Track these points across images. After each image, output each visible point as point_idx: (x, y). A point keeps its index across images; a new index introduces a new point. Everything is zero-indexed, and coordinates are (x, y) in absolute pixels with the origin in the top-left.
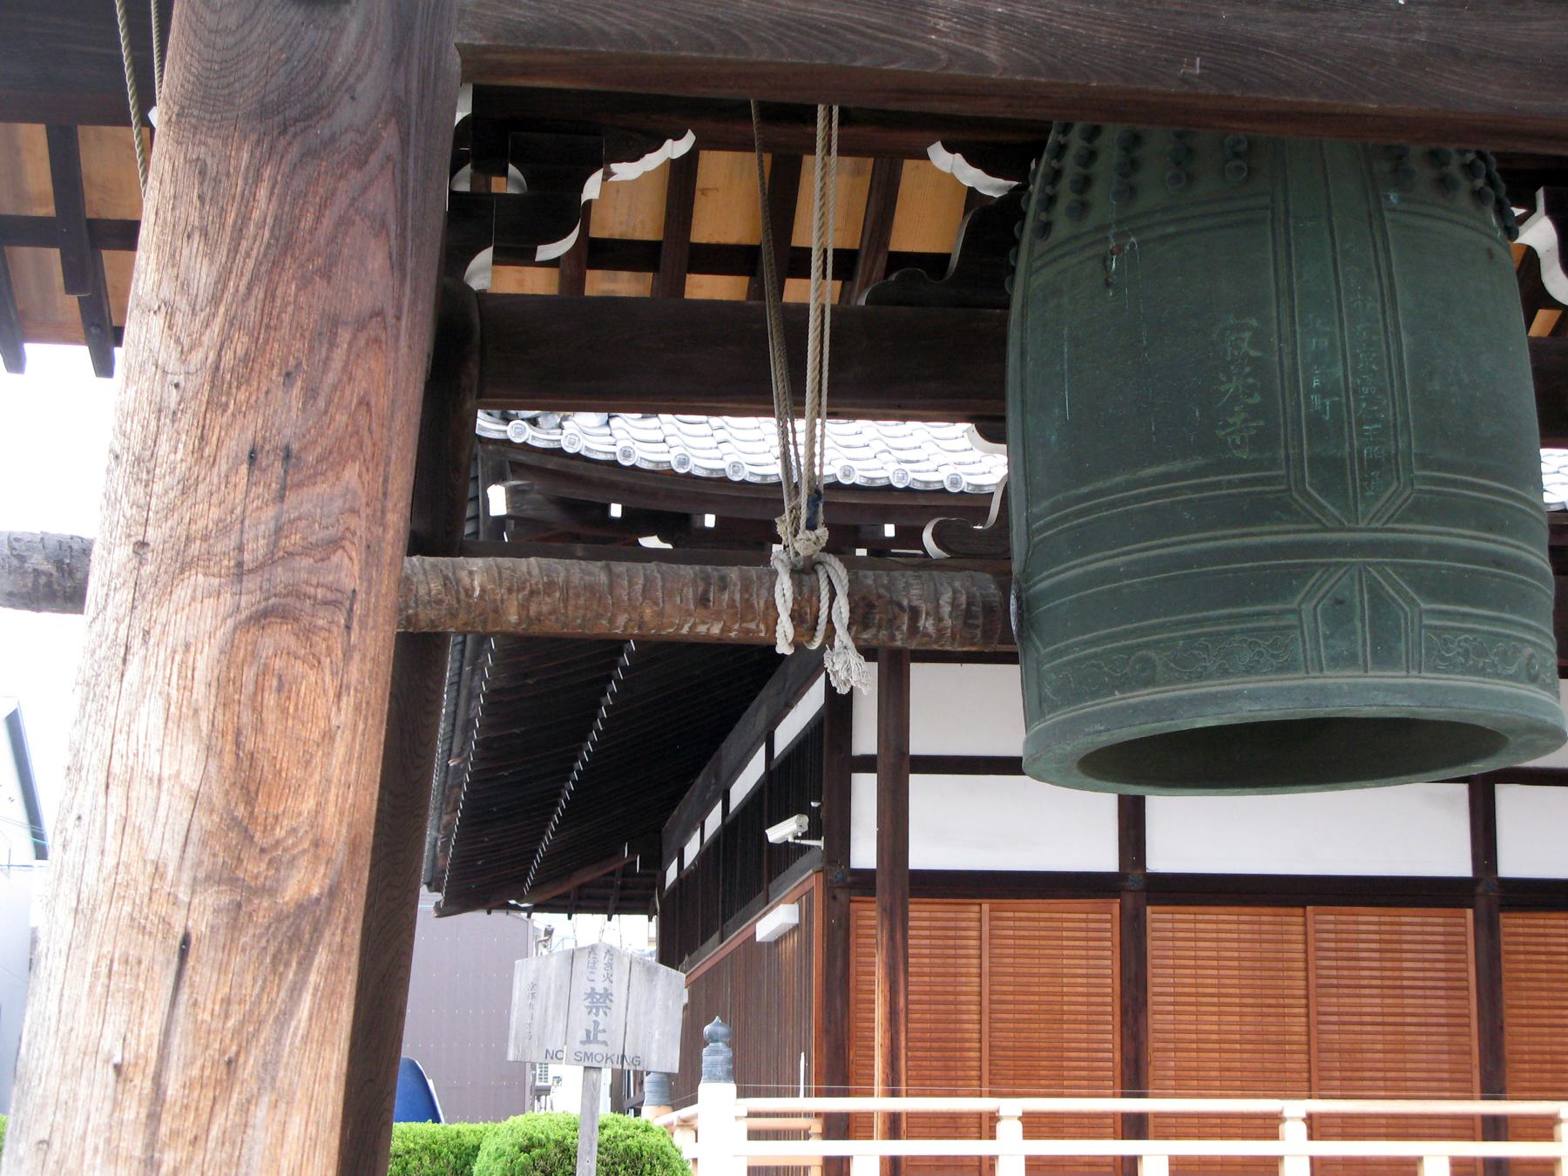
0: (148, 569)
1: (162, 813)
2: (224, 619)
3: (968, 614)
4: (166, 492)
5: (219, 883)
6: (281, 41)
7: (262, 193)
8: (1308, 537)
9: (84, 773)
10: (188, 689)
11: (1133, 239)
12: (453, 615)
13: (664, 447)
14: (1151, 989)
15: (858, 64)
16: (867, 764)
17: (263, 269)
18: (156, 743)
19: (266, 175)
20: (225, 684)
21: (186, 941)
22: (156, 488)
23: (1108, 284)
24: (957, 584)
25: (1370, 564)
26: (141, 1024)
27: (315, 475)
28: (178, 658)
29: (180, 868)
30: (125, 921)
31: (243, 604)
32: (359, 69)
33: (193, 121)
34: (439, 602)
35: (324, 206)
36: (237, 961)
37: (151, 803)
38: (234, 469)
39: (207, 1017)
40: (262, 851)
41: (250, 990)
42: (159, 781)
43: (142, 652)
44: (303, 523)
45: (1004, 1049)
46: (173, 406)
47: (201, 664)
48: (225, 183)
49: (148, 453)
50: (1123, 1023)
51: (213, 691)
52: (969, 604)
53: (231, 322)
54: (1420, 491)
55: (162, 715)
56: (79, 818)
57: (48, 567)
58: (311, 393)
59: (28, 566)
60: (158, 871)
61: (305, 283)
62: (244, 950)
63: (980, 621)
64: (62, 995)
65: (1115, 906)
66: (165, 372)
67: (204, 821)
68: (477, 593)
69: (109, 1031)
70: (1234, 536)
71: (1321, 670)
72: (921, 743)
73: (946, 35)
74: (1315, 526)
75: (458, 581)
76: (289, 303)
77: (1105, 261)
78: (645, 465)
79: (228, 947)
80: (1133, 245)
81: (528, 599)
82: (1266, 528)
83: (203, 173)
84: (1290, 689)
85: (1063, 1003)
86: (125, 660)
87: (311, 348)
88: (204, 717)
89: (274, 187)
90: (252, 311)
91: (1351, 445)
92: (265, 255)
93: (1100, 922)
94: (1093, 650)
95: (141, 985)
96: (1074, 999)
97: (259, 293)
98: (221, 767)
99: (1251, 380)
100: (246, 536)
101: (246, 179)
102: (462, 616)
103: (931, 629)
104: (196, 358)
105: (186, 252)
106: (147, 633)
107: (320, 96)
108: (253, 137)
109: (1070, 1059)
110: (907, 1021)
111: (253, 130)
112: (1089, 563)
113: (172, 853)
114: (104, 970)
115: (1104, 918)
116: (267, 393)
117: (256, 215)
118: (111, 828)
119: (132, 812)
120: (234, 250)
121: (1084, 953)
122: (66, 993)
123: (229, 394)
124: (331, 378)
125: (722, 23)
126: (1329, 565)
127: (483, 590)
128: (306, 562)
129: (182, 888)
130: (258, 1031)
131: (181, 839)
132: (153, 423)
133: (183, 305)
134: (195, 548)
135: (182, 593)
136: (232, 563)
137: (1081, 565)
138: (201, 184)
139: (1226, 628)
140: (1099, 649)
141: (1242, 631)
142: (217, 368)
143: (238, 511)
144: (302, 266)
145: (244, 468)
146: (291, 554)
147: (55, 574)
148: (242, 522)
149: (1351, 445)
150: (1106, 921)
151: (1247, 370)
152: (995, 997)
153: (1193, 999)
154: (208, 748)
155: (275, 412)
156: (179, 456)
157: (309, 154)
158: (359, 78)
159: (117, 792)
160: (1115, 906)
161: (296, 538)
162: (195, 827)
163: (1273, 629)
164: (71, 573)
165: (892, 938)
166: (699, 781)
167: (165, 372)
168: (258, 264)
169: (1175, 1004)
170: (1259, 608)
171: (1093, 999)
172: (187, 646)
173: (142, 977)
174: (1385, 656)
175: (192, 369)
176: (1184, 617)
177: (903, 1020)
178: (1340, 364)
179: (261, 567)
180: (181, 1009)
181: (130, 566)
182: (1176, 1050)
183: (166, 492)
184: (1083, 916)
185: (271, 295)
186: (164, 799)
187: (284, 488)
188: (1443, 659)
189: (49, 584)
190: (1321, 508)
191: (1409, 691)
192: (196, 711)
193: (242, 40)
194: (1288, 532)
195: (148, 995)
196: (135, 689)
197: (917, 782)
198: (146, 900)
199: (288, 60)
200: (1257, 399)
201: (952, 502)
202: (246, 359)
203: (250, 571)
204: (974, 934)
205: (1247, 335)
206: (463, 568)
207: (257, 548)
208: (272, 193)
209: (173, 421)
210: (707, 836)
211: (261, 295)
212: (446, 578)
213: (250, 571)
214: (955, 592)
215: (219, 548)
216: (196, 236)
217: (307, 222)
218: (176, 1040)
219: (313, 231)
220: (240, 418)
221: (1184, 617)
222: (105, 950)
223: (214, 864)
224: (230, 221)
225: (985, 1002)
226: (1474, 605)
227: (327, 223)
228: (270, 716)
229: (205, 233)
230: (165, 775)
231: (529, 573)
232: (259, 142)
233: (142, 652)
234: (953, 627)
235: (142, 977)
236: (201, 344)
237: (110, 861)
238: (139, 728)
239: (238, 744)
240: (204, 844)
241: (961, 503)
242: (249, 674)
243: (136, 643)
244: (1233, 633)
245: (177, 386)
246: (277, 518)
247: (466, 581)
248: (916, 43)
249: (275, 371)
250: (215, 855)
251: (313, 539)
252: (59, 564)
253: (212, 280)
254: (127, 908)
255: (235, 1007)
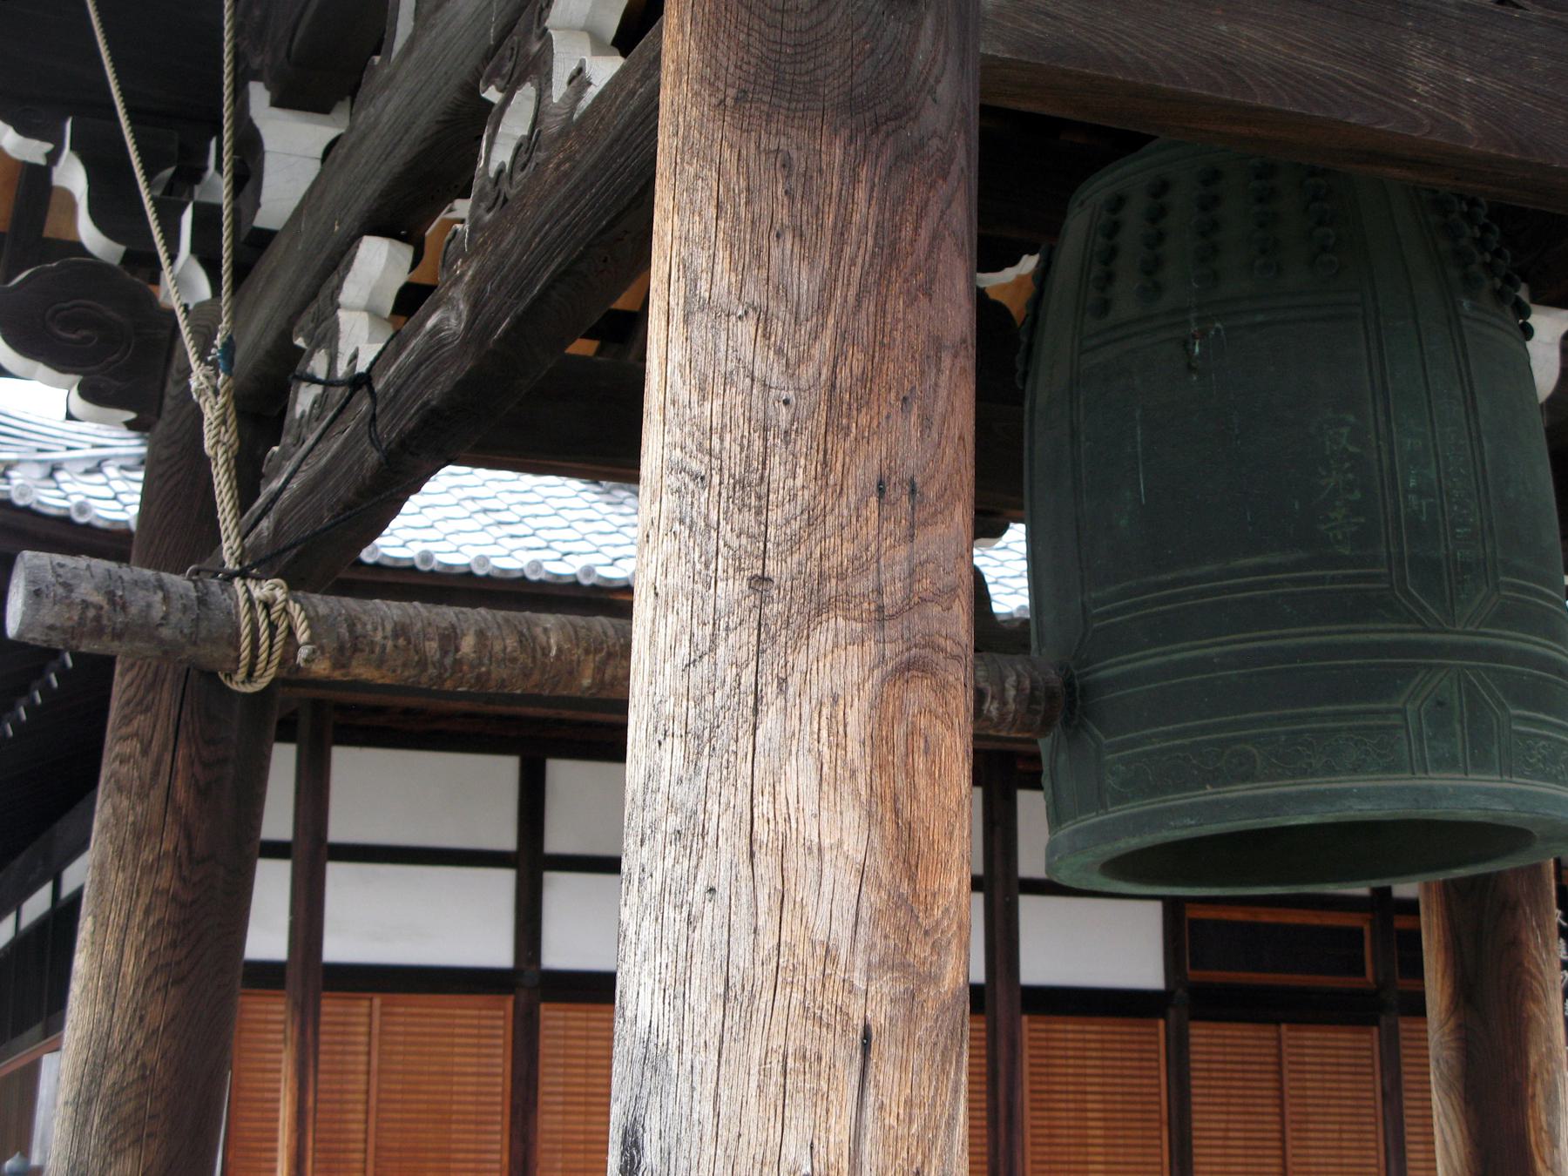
0: (773, 609)
1: (827, 888)
2: (871, 670)
3: (1032, 699)
4: (788, 522)
5: (892, 968)
6: (864, 30)
7: (861, 194)
8: (1412, 637)
9: (710, 839)
10: (839, 746)
11: (1218, 325)
12: (526, 675)
13: (115, 505)
14: (542, 1089)
15: (1352, 121)
16: (276, 850)
17: (871, 279)
18: (811, 808)
19: (863, 175)
20: (878, 742)
21: (867, 1035)
22: (772, 516)
23: (1190, 368)
24: (1019, 667)
25: (1468, 668)
26: (827, 1130)
27: (935, 514)
28: (825, 711)
29: (853, 951)
30: (796, 1011)
31: (887, 653)
32: (936, 71)
33: (765, 108)
34: (514, 660)
35: (920, 216)
36: (916, 1057)
37: (812, 876)
38: (863, 501)
39: (894, 1122)
40: (926, 933)
41: (927, 1093)
42: (820, 850)
43: (780, 702)
44: (931, 566)
45: (390, 1150)
46: (783, 425)
47: (852, 718)
48: (817, 182)
49: (755, 477)
50: (512, 1123)
51: (868, 750)
52: (1033, 689)
53: (842, 336)
54: (1506, 597)
55: (815, 777)
56: (712, 890)
57: (97, 598)
58: (926, 422)
59: (77, 596)
60: (829, 954)
61: (911, 301)
62: (920, 1044)
63: (1041, 708)
64: (717, 1095)
65: (509, 1002)
66: (766, 387)
67: (873, 897)
68: (554, 652)
69: (790, 1138)
70: (1339, 632)
71: (1426, 772)
72: (339, 831)
73: (1425, 99)
74: (1418, 626)
75: (534, 639)
76: (898, 320)
77: (1186, 344)
78: (100, 524)
79: (907, 1041)
80: (1218, 330)
81: (605, 662)
82: (1371, 626)
83: (787, 165)
84: (1401, 790)
85: (452, 1102)
86: (756, 711)
87: (922, 372)
88: (862, 779)
89: (872, 190)
90: (864, 324)
91: (1447, 547)
92: (871, 265)
93: (493, 1019)
94: (1178, 742)
95: (824, 1086)
96: (462, 1098)
97: (869, 306)
98: (883, 837)
99: (1350, 476)
100: (883, 577)
101: (842, 177)
102: (536, 676)
103: (994, 713)
104: (807, 373)
105: (775, 253)
106: (783, 682)
107: (907, 95)
108: (845, 133)
109: (456, 1161)
110: (315, 1122)
111: (843, 124)
112: (1173, 652)
113: (843, 933)
114: (777, 1068)
115: (496, 1016)
116: (888, 417)
117: (856, 218)
118: (763, 904)
119: (790, 885)
120: (837, 255)
121: (474, 1050)
122: (724, 1093)
123: (849, 416)
124: (941, 406)
125: (1225, 62)
126: (1430, 667)
127: (560, 650)
128: (935, 610)
129: (856, 974)
130: (935, 1136)
131: (852, 920)
132: (757, 445)
133: (781, 311)
134: (832, 586)
135: (822, 638)
136: (873, 607)
137: (1164, 654)
138: (788, 177)
139: (1331, 725)
140: (1186, 741)
141: (1350, 729)
142: (833, 386)
143: (873, 548)
144: (906, 281)
145: (874, 500)
146: (923, 600)
147: (106, 607)
148: (878, 561)
149: (1447, 547)
150: (498, 1018)
151: (1347, 465)
152: (383, 1096)
153: (582, 1099)
154: (870, 815)
155: (897, 439)
156: (799, 482)
157: (901, 158)
158: (938, 81)
159: (766, 864)
160: (509, 1002)
161: (926, 583)
162: (865, 904)
163: (1379, 727)
164: (124, 608)
165: (302, 1033)
166: (18, 863)
167: (766, 387)
168: (865, 275)
169: (564, 1103)
170: (1363, 706)
171: (482, 1098)
172: (835, 700)
173: (824, 1076)
174: (1481, 764)
175: (803, 384)
176: (1288, 712)
177: (310, 1120)
178: (1434, 465)
179: (900, 612)
180: (869, 1113)
181: (748, 603)
182: (565, 1151)
183: (788, 522)
184: (476, 1012)
185: (881, 310)
186: (828, 870)
187: (912, 526)
188: (1529, 765)
189: (98, 618)
190: (1423, 609)
191: (1504, 795)
192: (853, 773)
193: (820, 23)
194: (1392, 631)
195: (832, 1096)
196: (775, 745)
197: (336, 873)
198: (819, 988)
199: (873, 51)
200: (1357, 495)
201: (420, 581)
202: (864, 379)
203: (891, 617)
204: (363, 1029)
205: (1345, 430)
206: (537, 625)
207: (894, 595)
208: (871, 197)
209: (787, 444)
210: (11, 918)
211: (872, 309)
212: (521, 634)
213: (891, 617)
214: (1018, 676)
215: (857, 589)
216: (788, 237)
217: (907, 232)
218: (867, 1147)
219: (913, 241)
220: (863, 446)
221: (1288, 712)
222: (774, 1044)
223: (887, 947)
224: (829, 222)
225: (373, 1102)
226: (1547, 713)
227: (924, 234)
228: (922, 782)
229: (799, 234)
230: (826, 842)
231: (605, 633)
232: (851, 140)
233: (780, 702)
234: (1016, 711)
235: (824, 1076)
236: (810, 358)
237: (768, 941)
238: (788, 788)
239: (896, 812)
240: (875, 924)
241: (429, 582)
242: (900, 731)
243: (770, 692)
244: (1337, 730)
245: (786, 402)
246: (909, 559)
247: (542, 638)
248: (1401, 106)
249: (893, 394)
250: (886, 937)
251: (940, 585)
252: (110, 595)
253: (815, 286)
254: (797, 996)
255: (916, 1111)
